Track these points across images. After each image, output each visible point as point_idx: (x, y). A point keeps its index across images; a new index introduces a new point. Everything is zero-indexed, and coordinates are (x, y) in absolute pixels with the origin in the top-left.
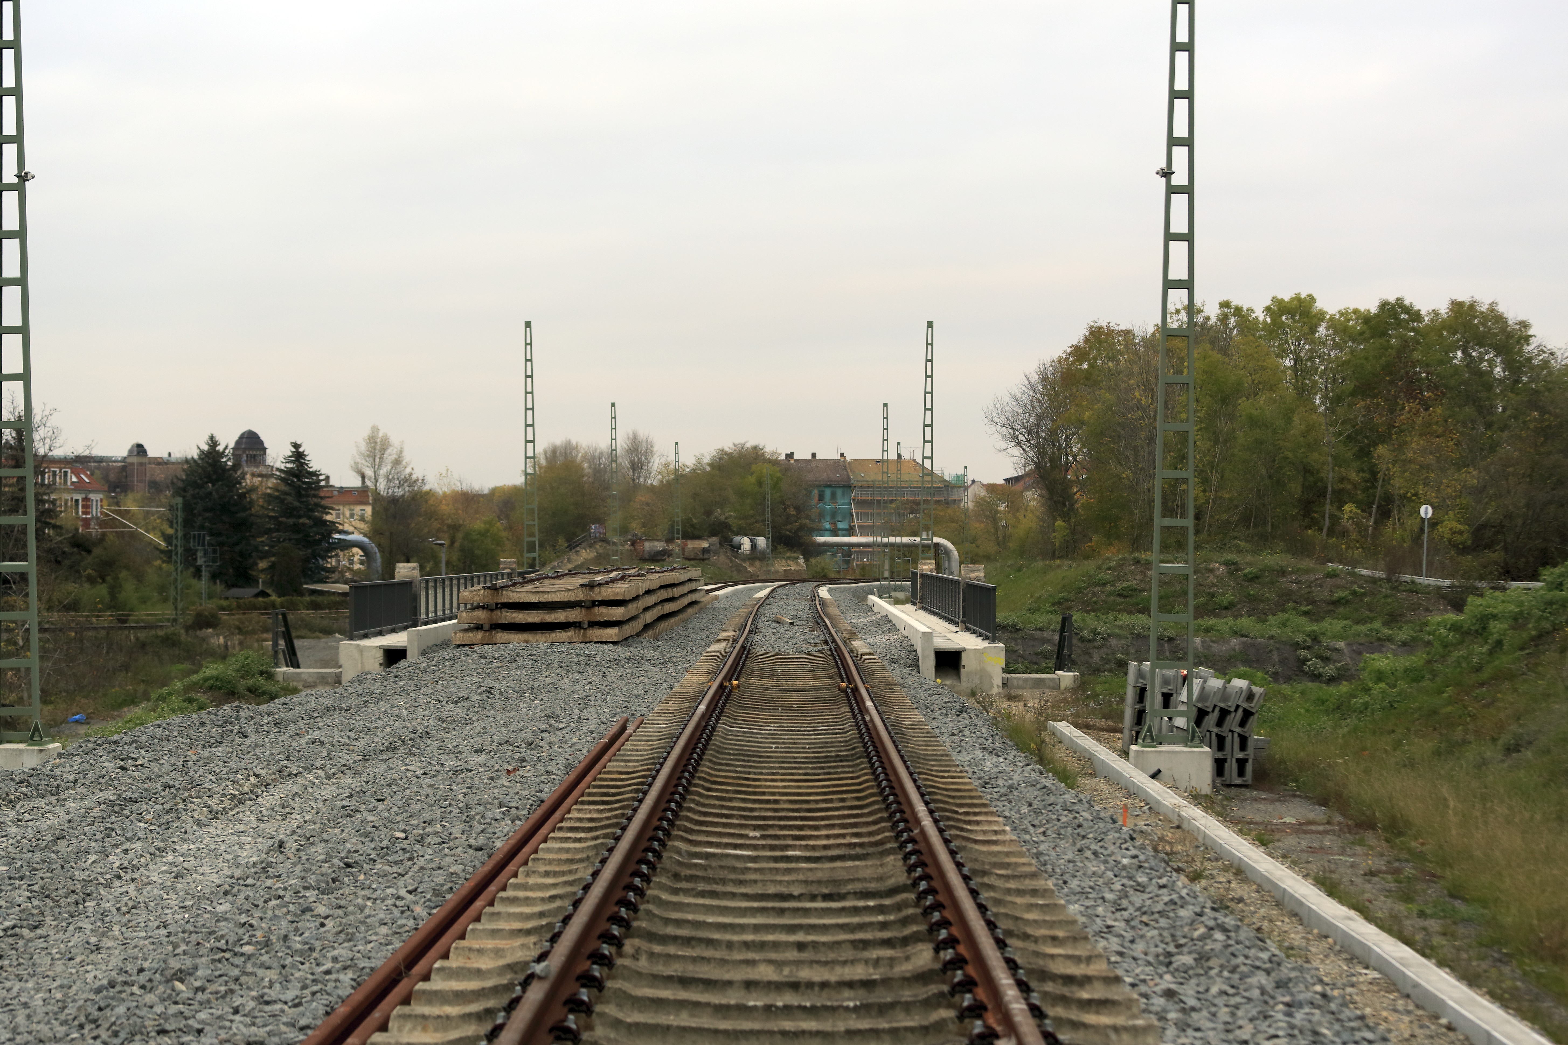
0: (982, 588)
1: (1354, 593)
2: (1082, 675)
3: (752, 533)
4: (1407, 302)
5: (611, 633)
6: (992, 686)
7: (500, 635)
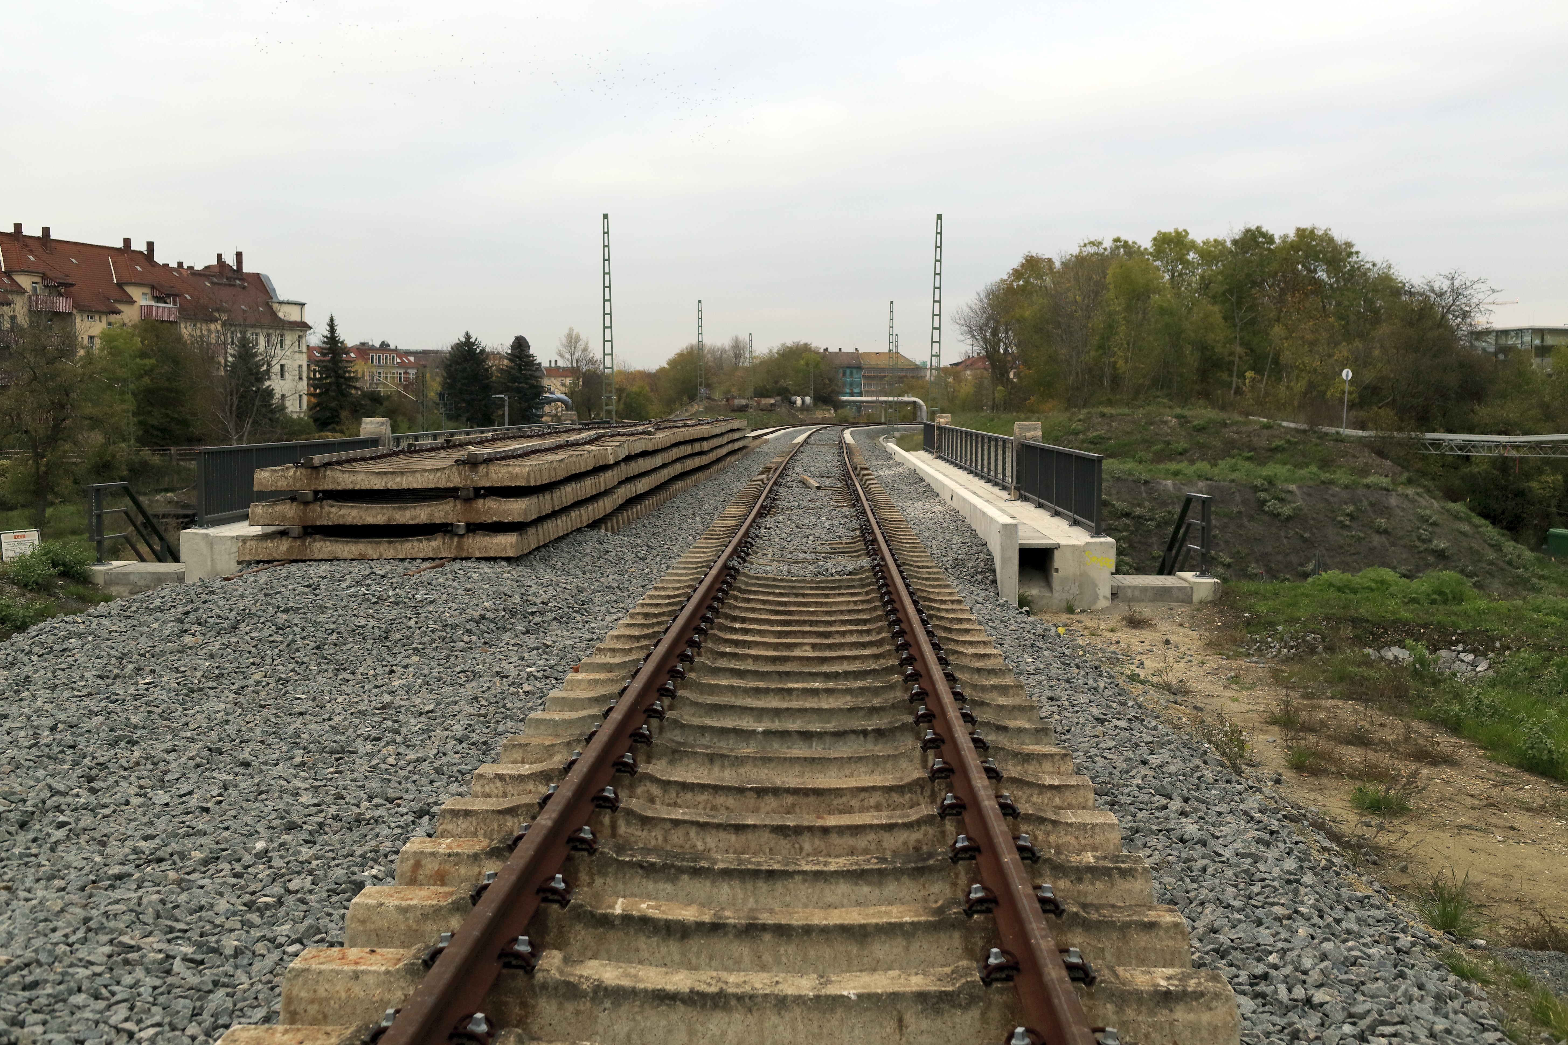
0: (1043, 450)
1: (1289, 442)
2: (1224, 580)
3: (803, 395)
4: (1264, 230)
5: (506, 542)
6: (1096, 598)
7: (318, 545)
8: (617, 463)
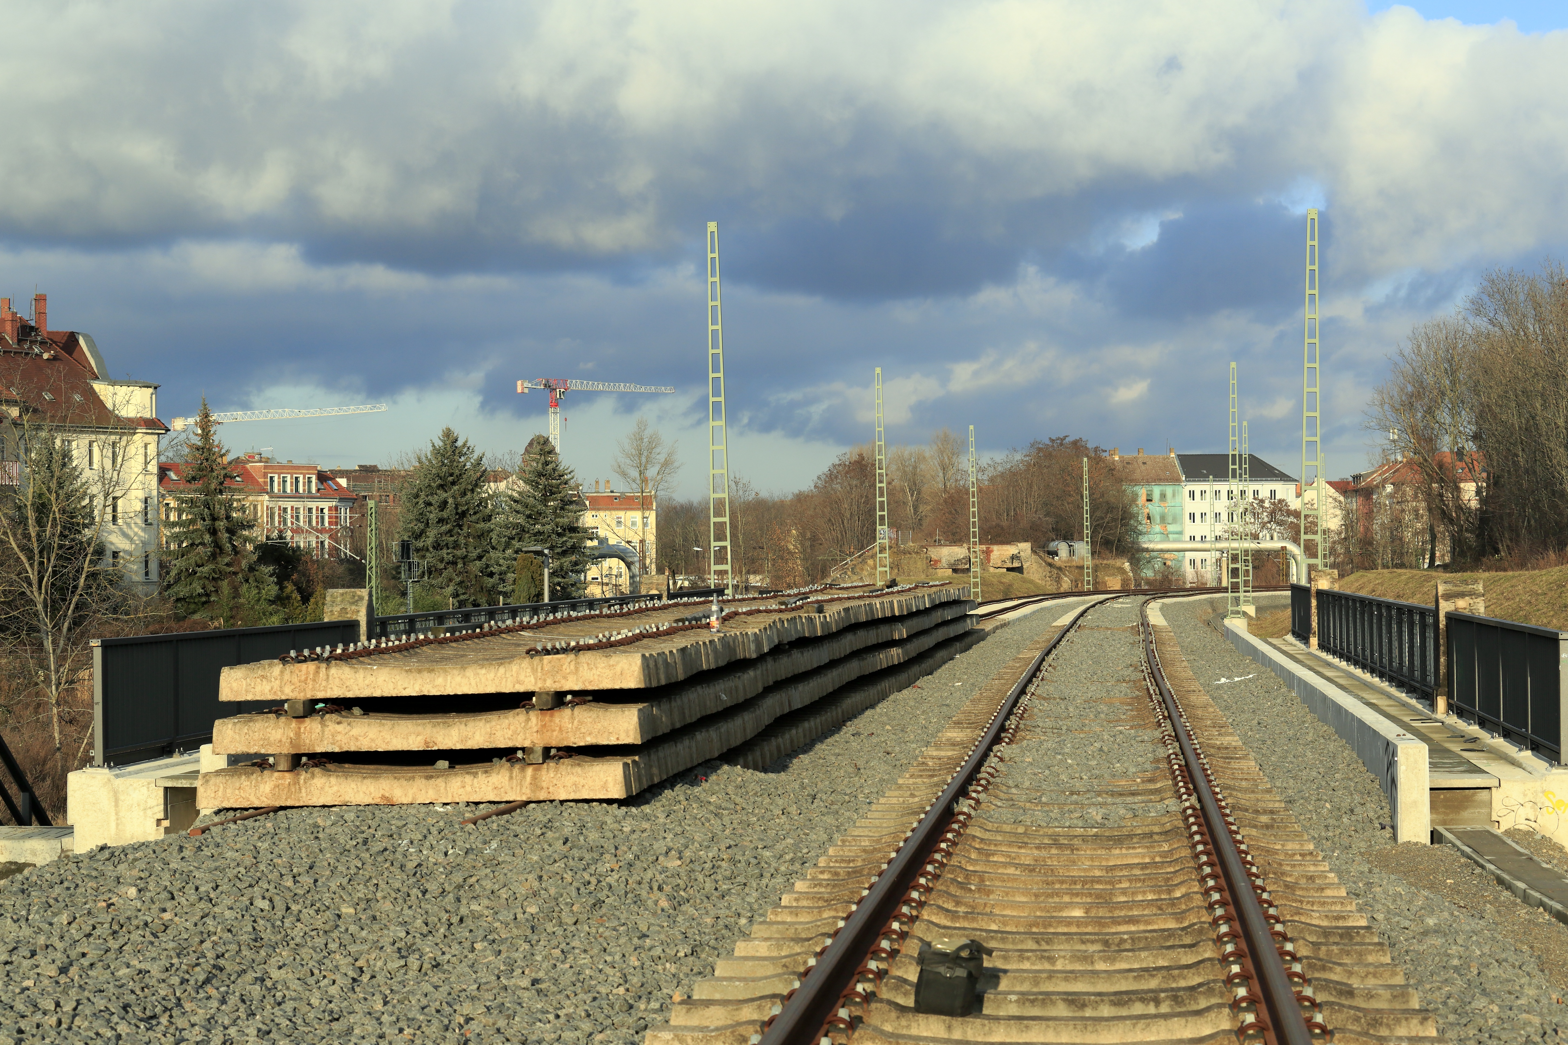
8: (762, 657)
